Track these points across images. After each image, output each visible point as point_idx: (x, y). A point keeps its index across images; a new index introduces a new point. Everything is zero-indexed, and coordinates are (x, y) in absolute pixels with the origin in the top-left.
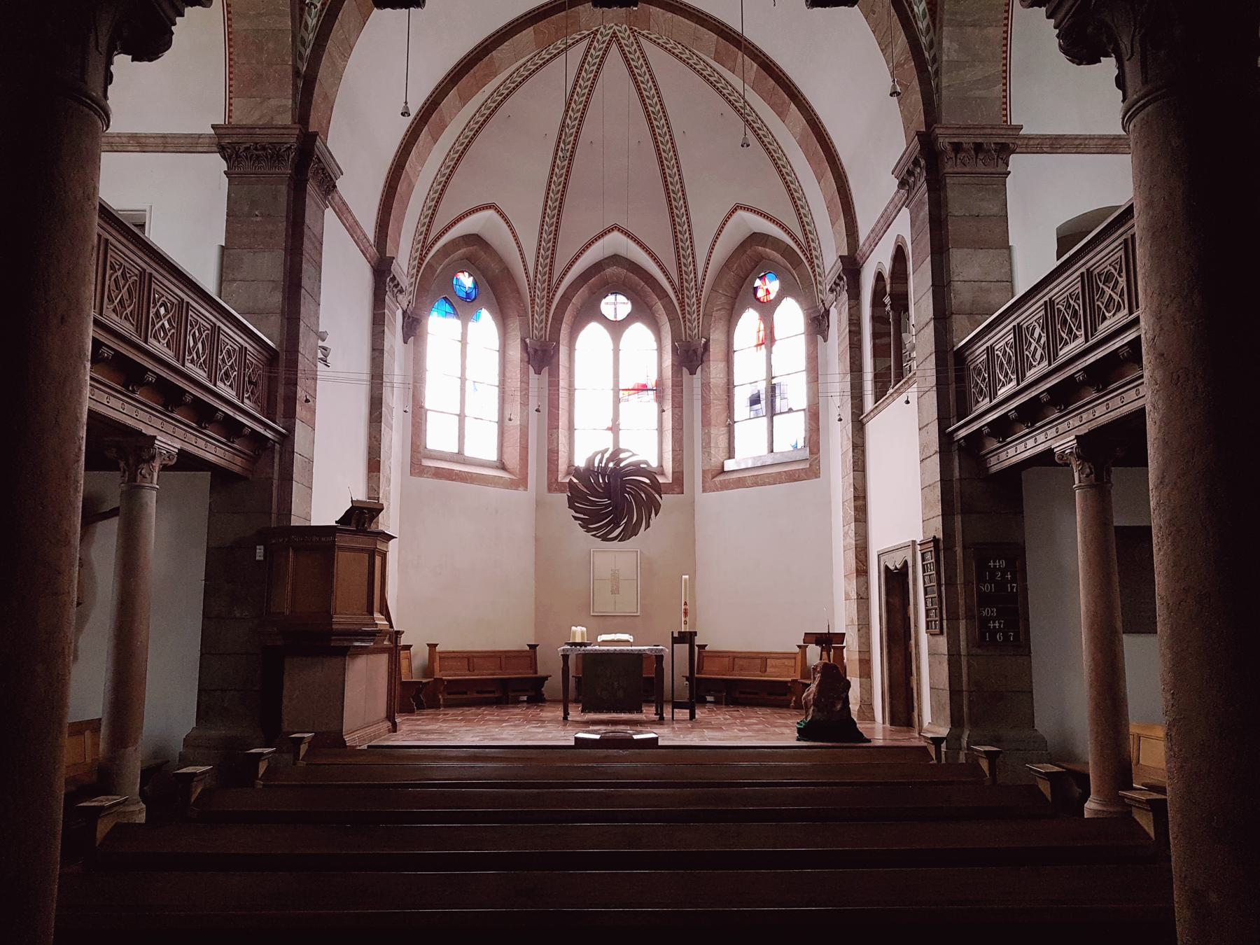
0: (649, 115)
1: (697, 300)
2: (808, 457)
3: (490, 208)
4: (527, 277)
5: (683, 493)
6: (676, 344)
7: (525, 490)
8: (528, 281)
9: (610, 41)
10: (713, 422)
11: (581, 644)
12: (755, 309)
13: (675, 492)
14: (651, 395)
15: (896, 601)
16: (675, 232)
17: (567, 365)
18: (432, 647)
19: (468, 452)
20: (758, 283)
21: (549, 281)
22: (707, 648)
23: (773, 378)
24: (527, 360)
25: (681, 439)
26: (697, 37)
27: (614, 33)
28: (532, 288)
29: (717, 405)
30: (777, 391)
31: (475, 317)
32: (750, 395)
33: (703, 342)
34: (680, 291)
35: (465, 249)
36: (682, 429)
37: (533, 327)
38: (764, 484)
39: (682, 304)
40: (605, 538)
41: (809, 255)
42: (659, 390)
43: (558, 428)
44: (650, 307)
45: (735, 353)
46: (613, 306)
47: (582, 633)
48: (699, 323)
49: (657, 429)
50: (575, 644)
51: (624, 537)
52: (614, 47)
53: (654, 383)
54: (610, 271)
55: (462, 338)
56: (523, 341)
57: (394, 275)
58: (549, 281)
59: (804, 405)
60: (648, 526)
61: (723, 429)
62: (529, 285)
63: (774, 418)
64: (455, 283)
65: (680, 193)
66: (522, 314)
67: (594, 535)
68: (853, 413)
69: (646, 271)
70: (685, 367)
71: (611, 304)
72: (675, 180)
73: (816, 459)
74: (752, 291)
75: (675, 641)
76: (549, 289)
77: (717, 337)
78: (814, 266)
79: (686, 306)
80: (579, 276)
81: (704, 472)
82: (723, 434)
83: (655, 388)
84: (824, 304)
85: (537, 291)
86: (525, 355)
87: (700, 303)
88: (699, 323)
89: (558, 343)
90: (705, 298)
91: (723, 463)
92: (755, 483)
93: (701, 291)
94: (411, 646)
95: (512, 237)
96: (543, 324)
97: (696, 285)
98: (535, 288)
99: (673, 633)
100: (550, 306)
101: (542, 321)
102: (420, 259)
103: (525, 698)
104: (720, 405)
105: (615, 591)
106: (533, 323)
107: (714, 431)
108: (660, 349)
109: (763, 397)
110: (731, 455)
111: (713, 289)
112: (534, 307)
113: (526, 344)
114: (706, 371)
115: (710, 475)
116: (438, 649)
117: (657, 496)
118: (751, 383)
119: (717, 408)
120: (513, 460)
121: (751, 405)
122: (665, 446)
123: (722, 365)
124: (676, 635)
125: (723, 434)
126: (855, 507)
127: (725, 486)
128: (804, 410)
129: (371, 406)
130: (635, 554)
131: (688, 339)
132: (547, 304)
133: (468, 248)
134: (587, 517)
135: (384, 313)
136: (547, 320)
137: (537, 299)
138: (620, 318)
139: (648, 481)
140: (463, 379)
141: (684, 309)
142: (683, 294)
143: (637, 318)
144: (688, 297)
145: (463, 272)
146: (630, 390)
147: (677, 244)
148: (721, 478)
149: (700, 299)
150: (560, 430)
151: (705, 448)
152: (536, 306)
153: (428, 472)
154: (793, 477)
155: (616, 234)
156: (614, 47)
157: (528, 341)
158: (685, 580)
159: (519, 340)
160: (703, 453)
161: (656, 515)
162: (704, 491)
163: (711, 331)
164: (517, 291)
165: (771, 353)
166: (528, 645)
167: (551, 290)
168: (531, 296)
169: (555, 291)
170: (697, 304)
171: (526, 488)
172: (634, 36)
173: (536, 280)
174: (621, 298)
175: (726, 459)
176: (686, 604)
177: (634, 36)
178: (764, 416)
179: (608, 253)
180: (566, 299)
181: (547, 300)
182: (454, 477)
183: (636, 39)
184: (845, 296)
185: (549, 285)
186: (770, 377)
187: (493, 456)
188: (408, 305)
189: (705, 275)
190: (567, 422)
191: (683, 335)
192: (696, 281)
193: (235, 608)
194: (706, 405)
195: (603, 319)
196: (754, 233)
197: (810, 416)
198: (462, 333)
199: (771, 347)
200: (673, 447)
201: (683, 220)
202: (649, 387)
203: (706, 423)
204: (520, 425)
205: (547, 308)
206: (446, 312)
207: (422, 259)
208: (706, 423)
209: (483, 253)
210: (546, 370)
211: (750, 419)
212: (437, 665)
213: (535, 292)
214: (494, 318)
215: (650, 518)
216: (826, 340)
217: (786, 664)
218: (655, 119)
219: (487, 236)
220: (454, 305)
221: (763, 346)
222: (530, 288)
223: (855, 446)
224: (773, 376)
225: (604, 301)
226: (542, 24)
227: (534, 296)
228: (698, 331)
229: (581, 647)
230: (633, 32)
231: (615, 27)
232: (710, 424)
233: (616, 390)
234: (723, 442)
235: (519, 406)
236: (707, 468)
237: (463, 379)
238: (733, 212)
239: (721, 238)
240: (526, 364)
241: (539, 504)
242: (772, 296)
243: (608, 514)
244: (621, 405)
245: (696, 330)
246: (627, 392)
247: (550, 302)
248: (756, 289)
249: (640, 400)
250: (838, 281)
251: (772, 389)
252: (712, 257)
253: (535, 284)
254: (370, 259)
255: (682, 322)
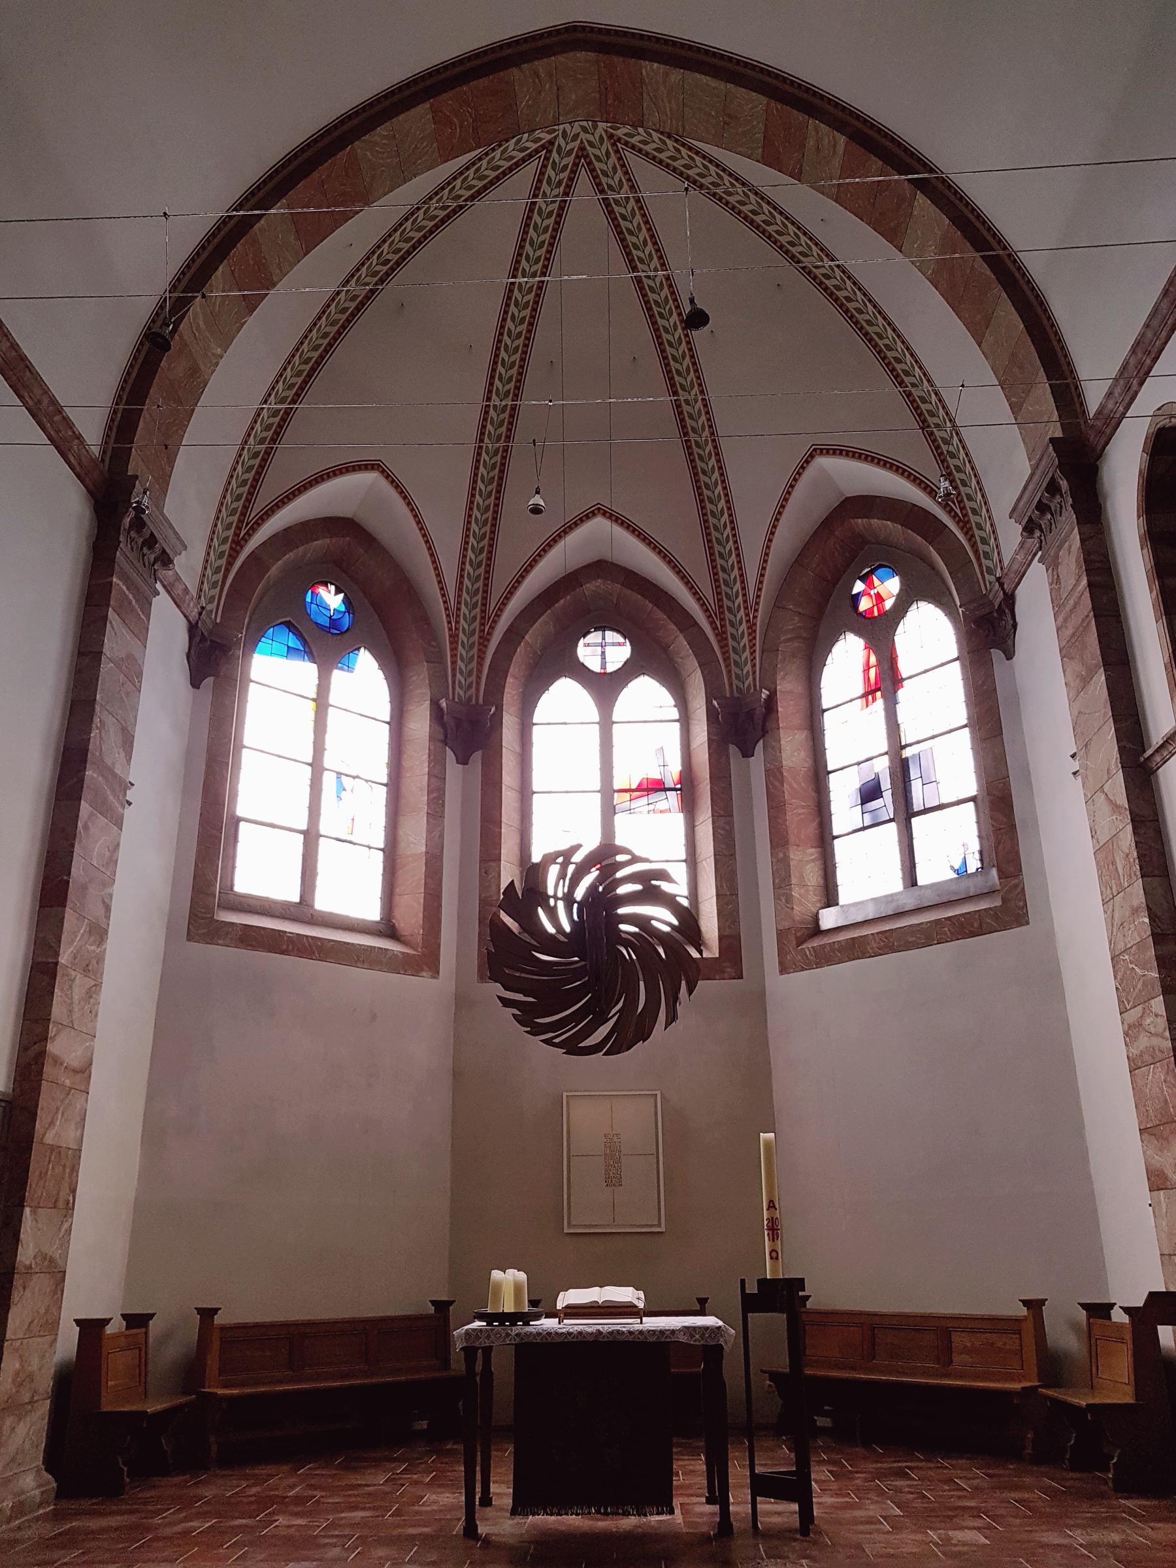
0: (650, 309)
1: (748, 628)
2: (998, 888)
3: (373, 469)
4: (443, 595)
5: (741, 977)
6: (715, 703)
7: (433, 977)
8: (445, 602)
9: (576, 165)
10: (792, 838)
11: (514, 1318)
12: (858, 633)
13: (726, 976)
14: (672, 800)
16: (705, 515)
17: (518, 749)
18: (207, 1314)
19: (323, 903)
20: (859, 587)
21: (484, 605)
23: (903, 747)
24: (441, 737)
25: (733, 873)
26: (730, 116)
27: (582, 148)
28: (453, 615)
29: (797, 807)
30: (914, 773)
31: (345, 660)
32: (858, 786)
33: (763, 696)
34: (717, 615)
35: (328, 541)
36: (733, 855)
37: (454, 682)
38: (908, 947)
39: (721, 636)
40: (572, 1048)
41: (958, 511)
42: (687, 787)
43: (498, 859)
44: (665, 649)
45: (826, 714)
46: (599, 649)
47: (518, 1288)
48: (754, 666)
49: (675, 706)
50: (502, 1317)
51: (620, 1043)
52: (583, 177)
53: (676, 776)
54: (592, 587)
55: (318, 694)
56: (435, 704)
57: (152, 534)
58: (484, 605)
59: (970, 786)
60: (672, 1018)
61: (812, 850)
62: (447, 609)
63: (913, 820)
64: (308, 599)
65: (710, 446)
66: (435, 658)
67: (547, 1042)
68: (1121, 750)
69: (655, 586)
71: (596, 645)
72: (700, 423)
73: (1016, 886)
74: (848, 602)
75: (750, 1304)
76: (483, 618)
77: (788, 686)
78: (971, 528)
79: (730, 640)
80: (538, 597)
81: (781, 934)
82: (813, 861)
83: (678, 786)
84: (1001, 585)
85: (462, 621)
86: (438, 728)
87: (755, 631)
88: (754, 666)
89: (500, 709)
90: (762, 621)
91: (817, 914)
92: (886, 946)
93: (756, 610)
95: (426, 550)
96: (474, 678)
97: (745, 601)
98: (458, 616)
99: (743, 1281)
100: (486, 646)
101: (470, 673)
102: (233, 541)
103: (424, 1425)
104: (803, 807)
105: (613, 1179)
106: (454, 676)
107: (795, 855)
108: (685, 721)
109: (886, 784)
110: (830, 897)
111: (778, 604)
112: (456, 649)
113: (441, 709)
115: (793, 938)
116: (218, 1320)
118: (859, 764)
119: (797, 812)
120: (410, 917)
121: (862, 804)
123: (801, 736)
124: (752, 1289)
125: (813, 861)
126: (1158, 958)
127: (824, 958)
128: (973, 799)
129: (63, 765)
130: (652, 1100)
131: (736, 694)
132: (480, 644)
133: (334, 540)
134: (531, 999)
135: (112, 582)
136: (480, 671)
137: (461, 635)
138: (611, 668)
140: (317, 767)
141: (727, 645)
142: (722, 620)
143: (642, 667)
144: (732, 624)
145: (325, 584)
146: (633, 791)
147: (708, 534)
148: (816, 943)
149: (755, 624)
150: (502, 862)
151: (780, 888)
152: (460, 647)
153: (227, 933)
154: (966, 928)
155: (599, 522)
156: (583, 177)
157: (443, 703)
158: (768, 1145)
159: (428, 702)
160: (777, 898)
162: (784, 970)
163: (779, 677)
164: (424, 620)
165: (896, 703)
167: (487, 621)
168: (450, 629)
169: (495, 622)
170: (749, 634)
171: (435, 972)
172: (617, 151)
173: (459, 603)
174: (612, 636)
175: (823, 908)
176: (771, 1205)
177: (617, 151)
178: (890, 820)
179: (588, 557)
180: (514, 635)
181: (480, 637)
182: (285, 947)
183: (620, 159)
184: (1069, 517)
185: (483, 611)
186: (896, 746)
187: (372, 912)
188: (200, 614)
189: (761, 582)
190: (516, 850)
191: (727, 687)
192: (744, 595)
194: (776, 807)
195: (581, 673)
196: (847, 498)
197: (991, 802)
198: (319, 686)
199: (895, 692)
200: (717, 892)
201: (716, 493)
202: (669, 783)
203: (779, 841)
204: (427, 853)
205: (479, 650)
206: (288, 647)
207: (238, 544)
208: (779, 841)
209: (361, 551)
210: (477, 756)
211: (864, 828)
212: (213, 1362)
213: (457, 622)
214: (382, 666)
215: (676, 999)
216: (1009, 655)
217: (999, 1344)
218: (661, 316)
219: (374, 523)
220: (305, 634)
222: (448, 616)
223: (1138, 822)
224: (903, 743)
225: (582, 642)
226: (448, 100)
227: (457, 629)
228: (754, 679)
229: (514, 1324)
230: (614, 140)
231: (583, 136)
232: (787, 843)
233: (607, 791)
234: (813, 876)
235: (425, 818)
236: (787, 924)
237: (317, 767)
238: (807, 462)
239: (783, 519)
240: (440, 744)
241: (462, 1002)
242: (888, 604)
243: (576, 995)
244: (617, 817)
245: (751, 678)
246: (627, 796)
247: (485, 640)
248: (856, 599)
249: (651, 807)
251: (901, 770)
252: (772, 549)
253: (459, 609)
254: (78, 468)
255: (723, 667)
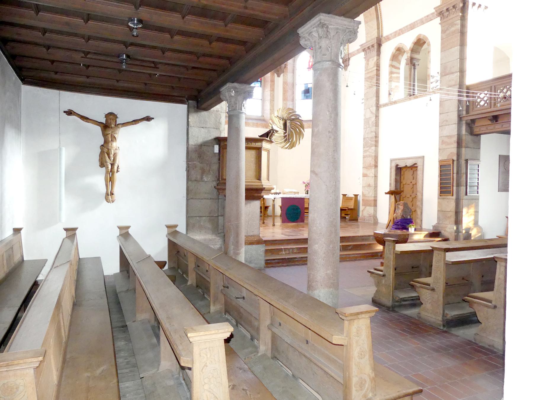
15: (398, 178)
22: (347, 196)
70: (276, 73)
94: (358, 195)
114: (285, 77)
117: (302, 129)
122: (474, 116)
139: (299, 124)
161: (302, 139)
166: (354, 195)
193: (204, 176)
221: (312, 69)
250: (371, 47)
